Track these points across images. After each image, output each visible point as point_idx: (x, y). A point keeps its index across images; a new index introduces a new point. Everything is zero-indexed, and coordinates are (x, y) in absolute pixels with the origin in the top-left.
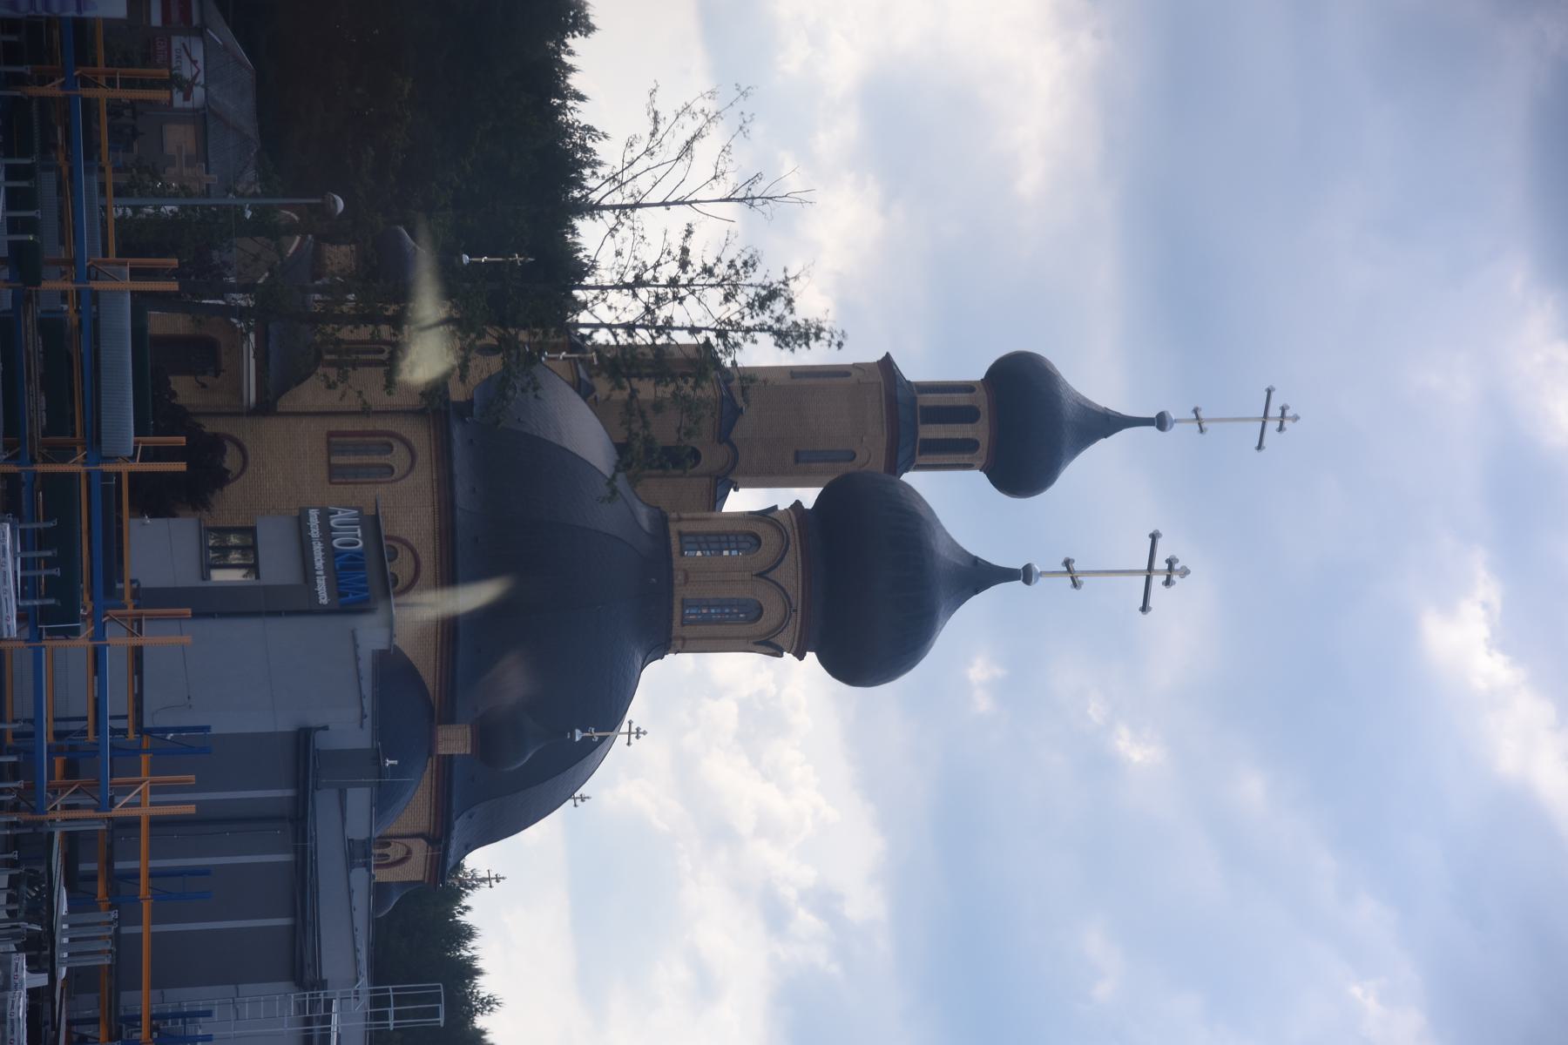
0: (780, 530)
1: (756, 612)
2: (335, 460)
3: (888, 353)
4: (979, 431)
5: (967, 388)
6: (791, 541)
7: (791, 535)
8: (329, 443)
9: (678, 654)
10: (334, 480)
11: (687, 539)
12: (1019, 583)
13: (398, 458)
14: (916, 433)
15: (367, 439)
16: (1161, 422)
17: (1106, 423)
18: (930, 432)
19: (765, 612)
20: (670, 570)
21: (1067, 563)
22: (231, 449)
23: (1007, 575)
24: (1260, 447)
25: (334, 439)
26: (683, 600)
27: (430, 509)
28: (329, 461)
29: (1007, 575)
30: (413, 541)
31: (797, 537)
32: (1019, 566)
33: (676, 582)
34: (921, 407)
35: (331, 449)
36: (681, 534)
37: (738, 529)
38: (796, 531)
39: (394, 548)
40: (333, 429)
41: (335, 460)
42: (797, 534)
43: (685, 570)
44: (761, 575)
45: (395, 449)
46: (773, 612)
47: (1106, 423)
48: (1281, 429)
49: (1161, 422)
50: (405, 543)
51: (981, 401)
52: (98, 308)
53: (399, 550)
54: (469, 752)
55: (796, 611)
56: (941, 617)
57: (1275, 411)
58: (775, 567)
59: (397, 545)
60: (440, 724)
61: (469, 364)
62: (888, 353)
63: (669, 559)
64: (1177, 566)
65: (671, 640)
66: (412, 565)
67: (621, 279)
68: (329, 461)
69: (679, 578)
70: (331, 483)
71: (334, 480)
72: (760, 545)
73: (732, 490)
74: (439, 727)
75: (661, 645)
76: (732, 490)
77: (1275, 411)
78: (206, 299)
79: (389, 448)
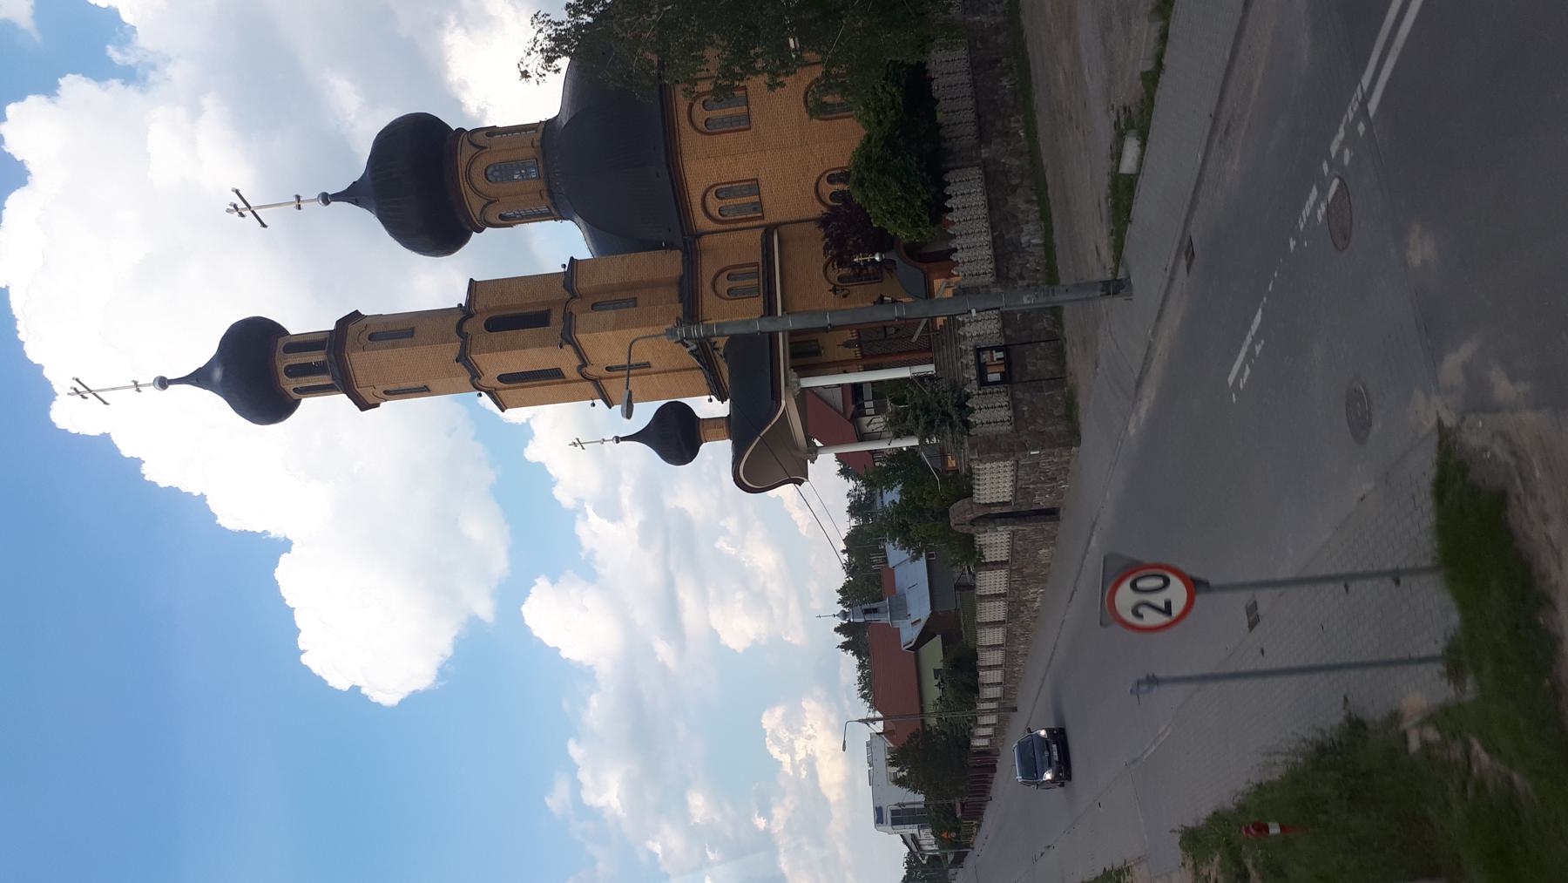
3: (7, 287)
4: (285, 361)
7: (466, 185)
16: (163, 383)
17: (199, 378)
18: (317, 357)
23: (338, 197)
28: (748, 109)
29: (338, 197)
32: (621, 443)
39: (721, 215)
44: (490, 202)
47: (199, 378)
49: (163, 383)
50: (703, 133)
51: (289, 385)
52: (995, 383)
58: (485, 206)
59: (728, 297)
61: (532, 453)
62: (7, 287)
65: (541, 146)
67: (141, 386)
68: (748, 109)
70: (757, 180)
73: (464, 305)
75: (549, 125)
76: (464, 305)
78: (1262, 316)
79: (729, 292)
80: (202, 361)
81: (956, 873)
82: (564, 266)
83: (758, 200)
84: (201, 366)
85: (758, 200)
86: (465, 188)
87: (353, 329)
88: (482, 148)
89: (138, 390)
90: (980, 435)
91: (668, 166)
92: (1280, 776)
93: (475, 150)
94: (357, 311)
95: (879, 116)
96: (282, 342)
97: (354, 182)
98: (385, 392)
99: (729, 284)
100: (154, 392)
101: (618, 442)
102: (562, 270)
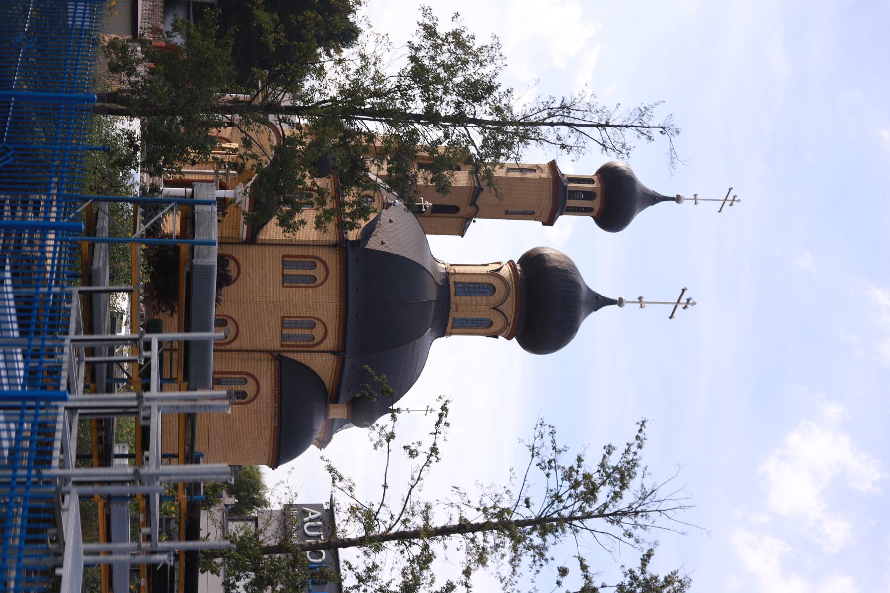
0: (505, 282)
1: (491, 324)
2: (287, 272)
4: (596, 204)
5: (589, 181)
6: (511, 290)
7: (511, 287)
8: (283, 261)
9: (452, 336)
10: (285, 284)
11: (458, 285)
12: (616, 306)
13: (319, 272)
14: (565, 203)
15: (303, 260)
16: (678, 199)
17: (654, 199)
19: (497, 288)
20: (449, 304)
21: (640, 298)
22: (232, 262)
23: (611, 302)
24: (720, 211)
25: (286, 259)
26: (454, 318)
27: (335, 304)
29: (611, 302)
30: (324, 319)
31: (514, 288)
33: (452, 310)
34: (569, 191)
35: (285, 265)
36: (456, 283)
37: (484, 281)
38: (514, 284)
40: (286, 254)
41: (287, 272)
42: (514, 286)
43: (456, 304)
45: (318, 266)
46: (499, 323)
47: (654, 199)
48: (731, 205)
49: (678, 199)
50: (317, 319)
51: (595, 178)
53: (317, 324)
54: (345, 418)
55: (509, 324)
56: (583, 314)
57: (730, 197)
59: (316, 321)
60: (330, 403)
63: (449, 298)
64: (691, 302)
66: (324, 330)
69: (453, 307)
71: (285, 284)
72: (493, 295)
74: (330, 404)
77: (730, 197)
79: (315, 266)
80: (650, 209)
81: (347, 563)
82: (474, 222)
83: (284, 330)
84: (651, 206)
85: (284, 330)
86: (511, 320)
87: (547, 205)
88: (494, 308)
89: (695, 195)
90: (418, 586)
91: (508, 295)
92: (171, 25)
93: (501, 308)
94: (462, 235)
95: (291, 81)
96: (595, 213)
97: (596, 311)
98: (535, 171)
99: (314, 332)
100: (686, 194)
101: (620, 299)
102: (476, 220)
